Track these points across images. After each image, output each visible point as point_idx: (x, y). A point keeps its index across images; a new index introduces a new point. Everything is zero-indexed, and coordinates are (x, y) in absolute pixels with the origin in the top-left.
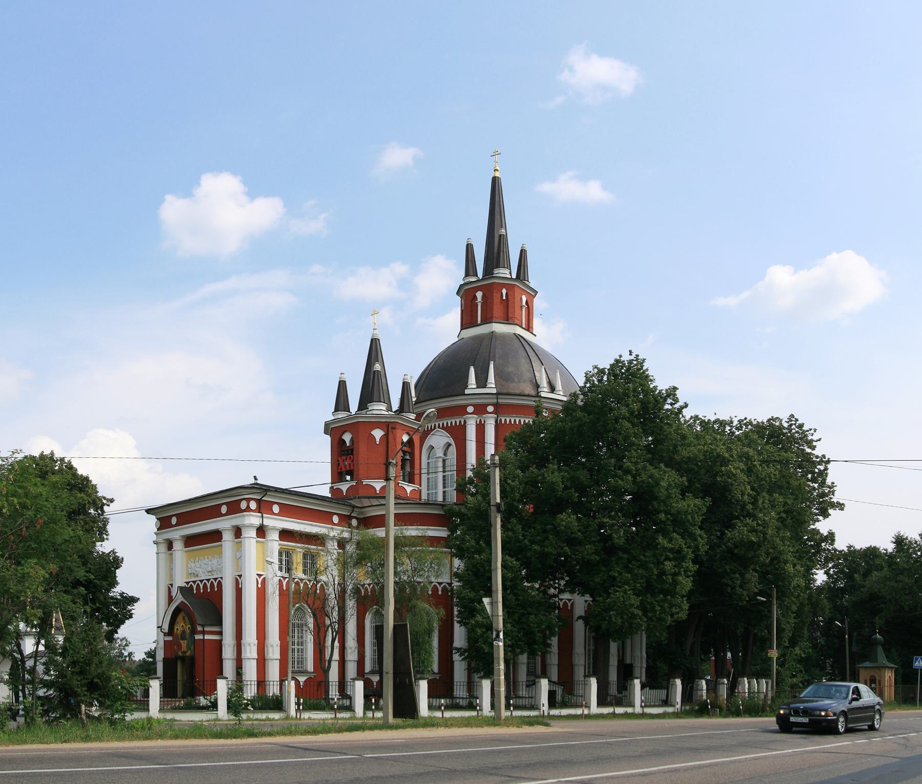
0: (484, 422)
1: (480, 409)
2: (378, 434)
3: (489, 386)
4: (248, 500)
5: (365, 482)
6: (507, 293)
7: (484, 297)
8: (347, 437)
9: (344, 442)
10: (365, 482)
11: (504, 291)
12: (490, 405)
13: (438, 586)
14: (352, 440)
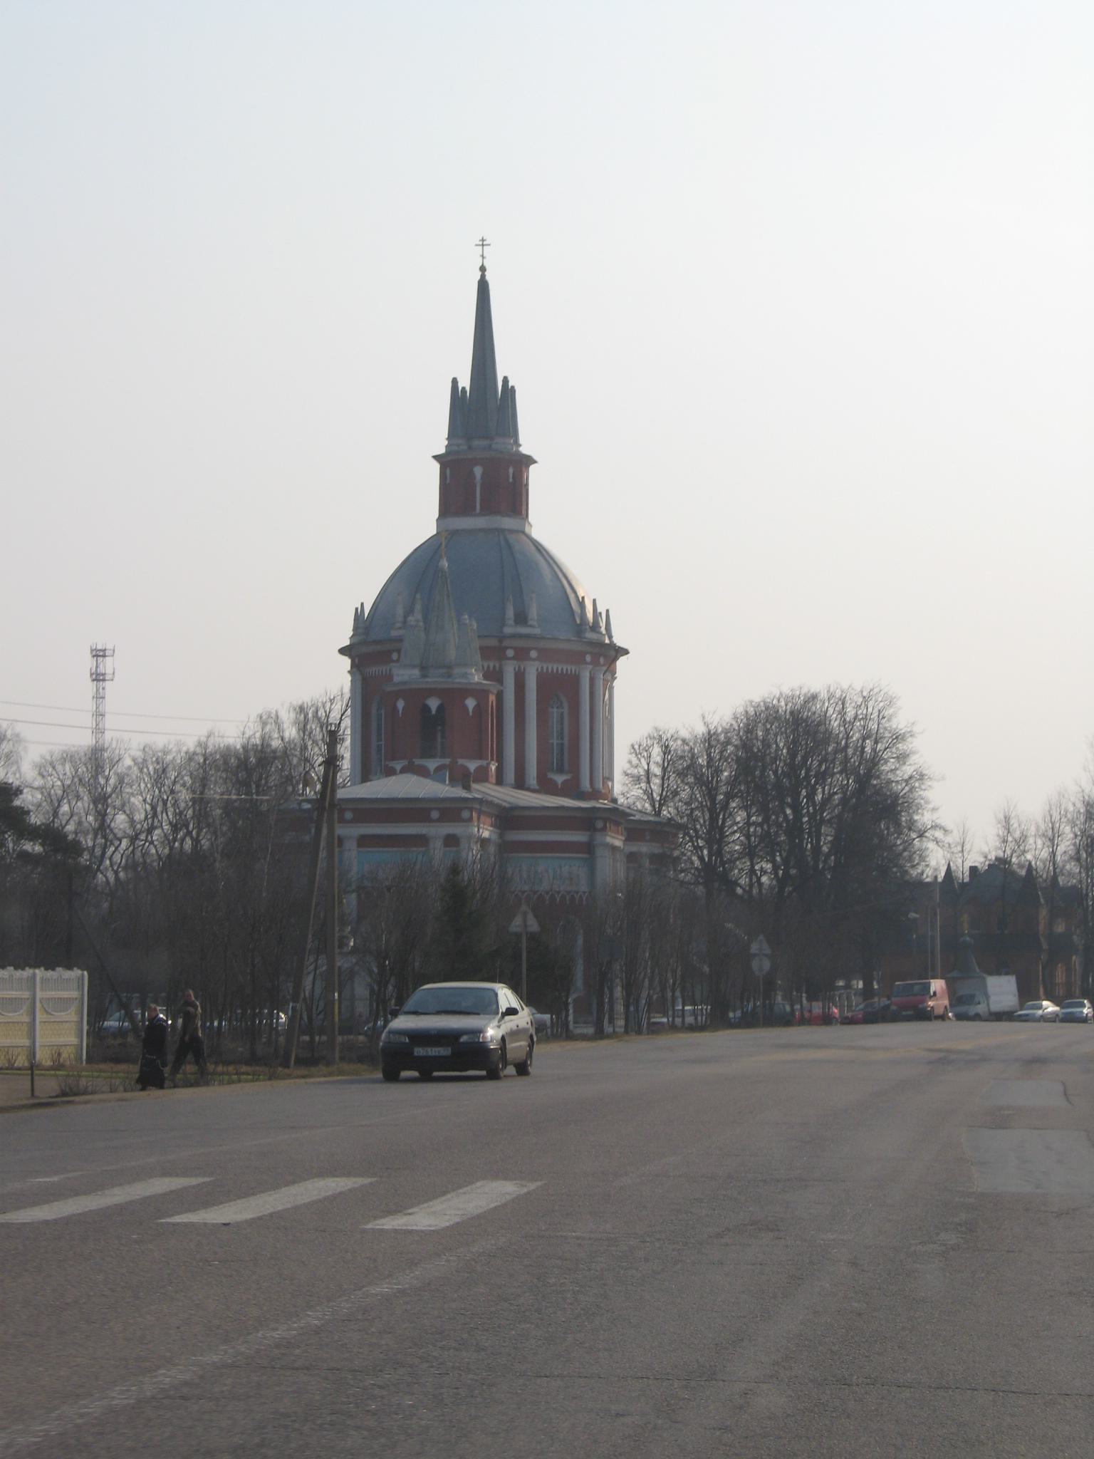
0: (524, 669)
1: (522, 654)
2: (471, 703)
3: (531, 623)
4: (471, 810)
5: (461, 761)
6: (513, 474)
7: (484, 475)
8: (433, 703)
9: (429, 710)
10: (461, 761)
11: (511, 470)
12: (511, 648)
13: (575, 895)
14: (440, 708)
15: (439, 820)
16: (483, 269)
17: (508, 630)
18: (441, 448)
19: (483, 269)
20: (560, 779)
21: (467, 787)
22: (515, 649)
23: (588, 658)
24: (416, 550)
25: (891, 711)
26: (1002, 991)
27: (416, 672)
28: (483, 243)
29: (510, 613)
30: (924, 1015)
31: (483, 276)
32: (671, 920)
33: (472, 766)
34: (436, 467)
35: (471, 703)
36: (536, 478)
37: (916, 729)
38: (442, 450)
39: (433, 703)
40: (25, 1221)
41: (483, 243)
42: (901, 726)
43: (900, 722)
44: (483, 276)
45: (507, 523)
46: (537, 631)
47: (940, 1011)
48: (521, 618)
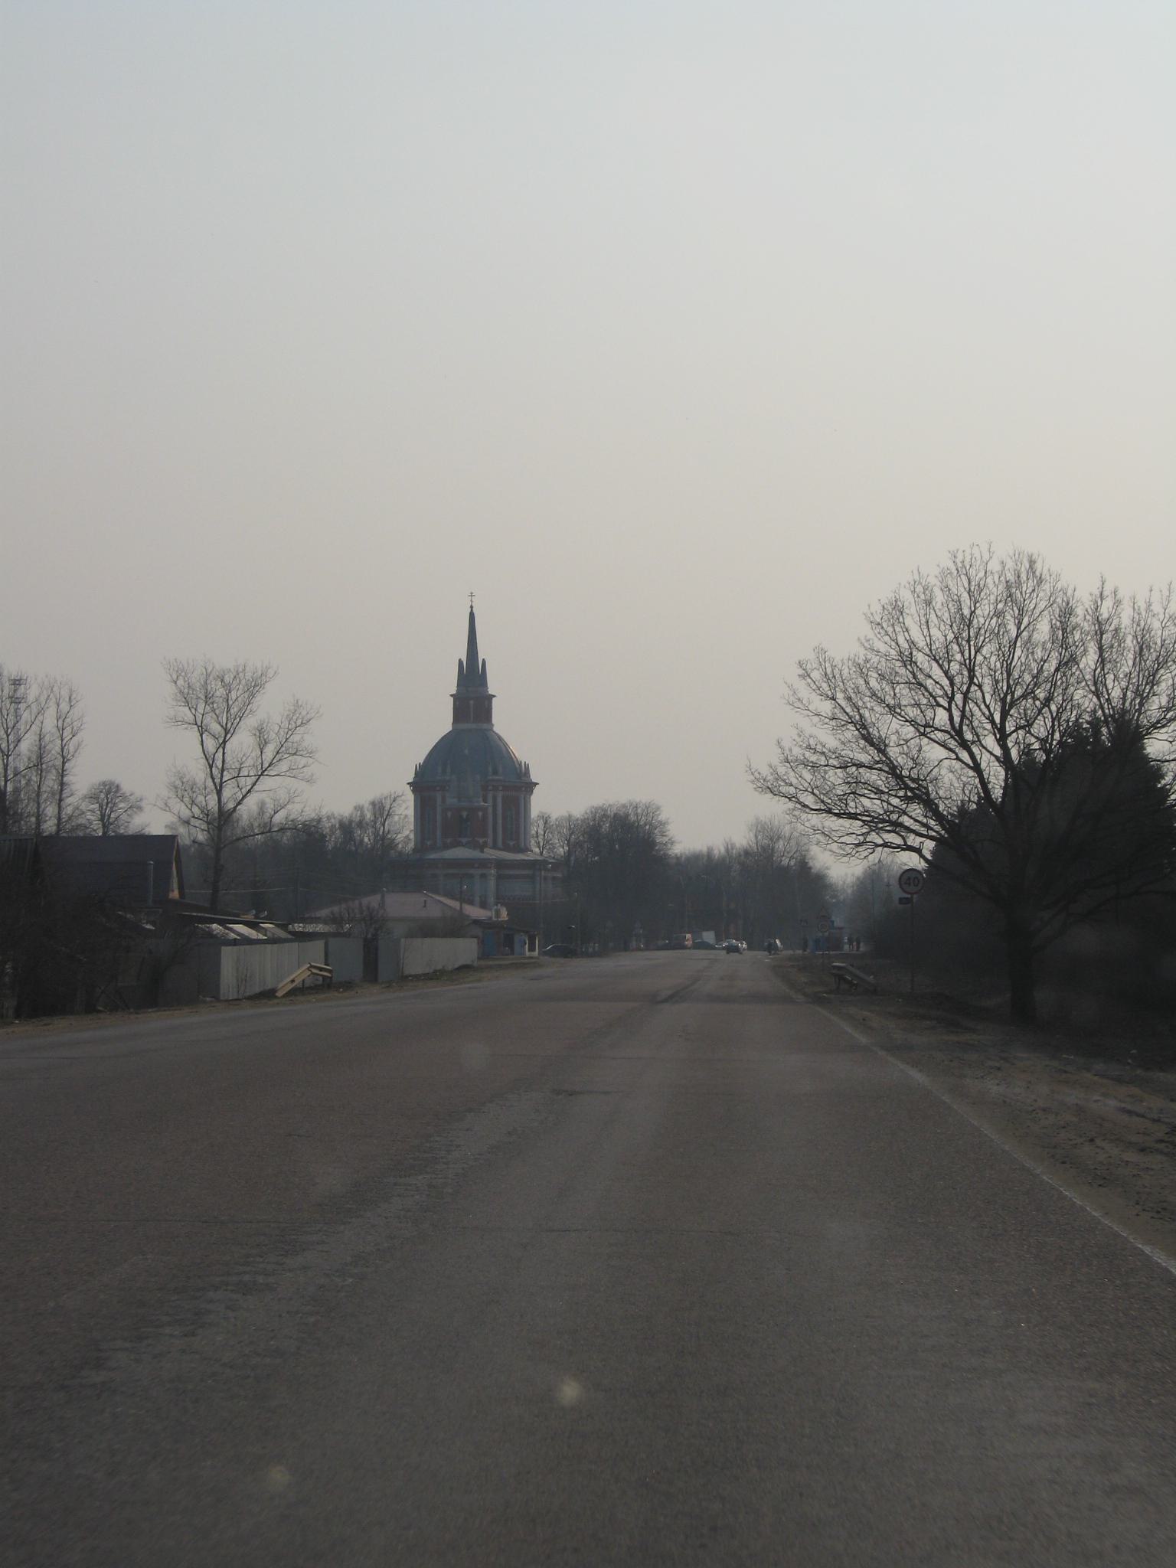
2: (480, 814)
8: (465, 814)
15: (478, 868)
16: (472, 607)
17: (490, 778)
18: (454, 692)
19: (472, 607)
20: (512, 843)
21: (482, 852)
22: (493, 786)
23: (523, 789)
24: (443, 738)
25: (658, 812)
26: (709, 937)
27: (455, 800)
28: (472, 595)
29: (490, 769)
30: (684, 947)
31: (472, 610)
32: (1065, 1056)
33: (481, 841)
34: (452, 699)
35: (480, 814)
36: (496, 705)
37: (670, 821)
38: (455, 692)
39: (465, 814)
40: (680, 951)
41: (472, 595)
42: (663, 819)
43: (662, 817)
44: (472, 610)
45: (485, 726)
46: (501, 778)
47: (689, 946)
48: (495, 772)
